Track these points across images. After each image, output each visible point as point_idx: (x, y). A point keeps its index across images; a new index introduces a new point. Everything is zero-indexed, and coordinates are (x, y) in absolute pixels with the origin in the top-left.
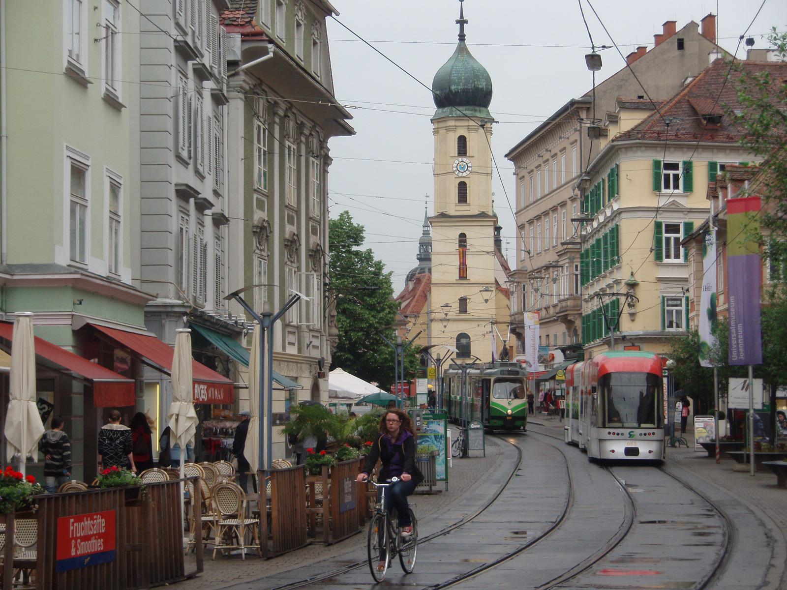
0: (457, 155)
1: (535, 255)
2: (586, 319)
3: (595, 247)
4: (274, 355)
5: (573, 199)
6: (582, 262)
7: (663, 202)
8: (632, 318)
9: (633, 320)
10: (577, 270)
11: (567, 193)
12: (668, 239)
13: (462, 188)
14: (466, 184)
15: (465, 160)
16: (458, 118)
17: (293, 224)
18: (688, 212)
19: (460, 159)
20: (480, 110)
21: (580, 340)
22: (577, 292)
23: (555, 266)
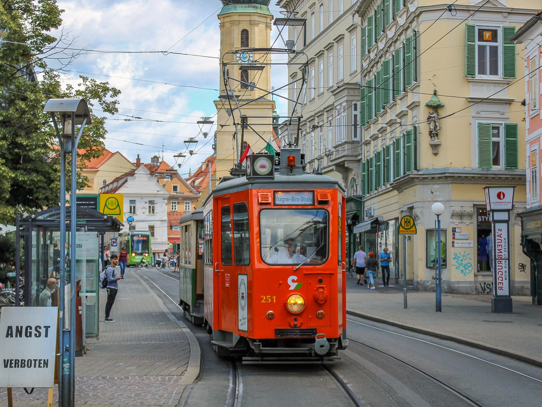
1: (308, 103)
5: (352, 29)
8: (436, 152)
9: (436, 154)
12: (482, 49)
18: (509, 13)
20: (261, 8)
22: (355, 136)
23: (330, 109)
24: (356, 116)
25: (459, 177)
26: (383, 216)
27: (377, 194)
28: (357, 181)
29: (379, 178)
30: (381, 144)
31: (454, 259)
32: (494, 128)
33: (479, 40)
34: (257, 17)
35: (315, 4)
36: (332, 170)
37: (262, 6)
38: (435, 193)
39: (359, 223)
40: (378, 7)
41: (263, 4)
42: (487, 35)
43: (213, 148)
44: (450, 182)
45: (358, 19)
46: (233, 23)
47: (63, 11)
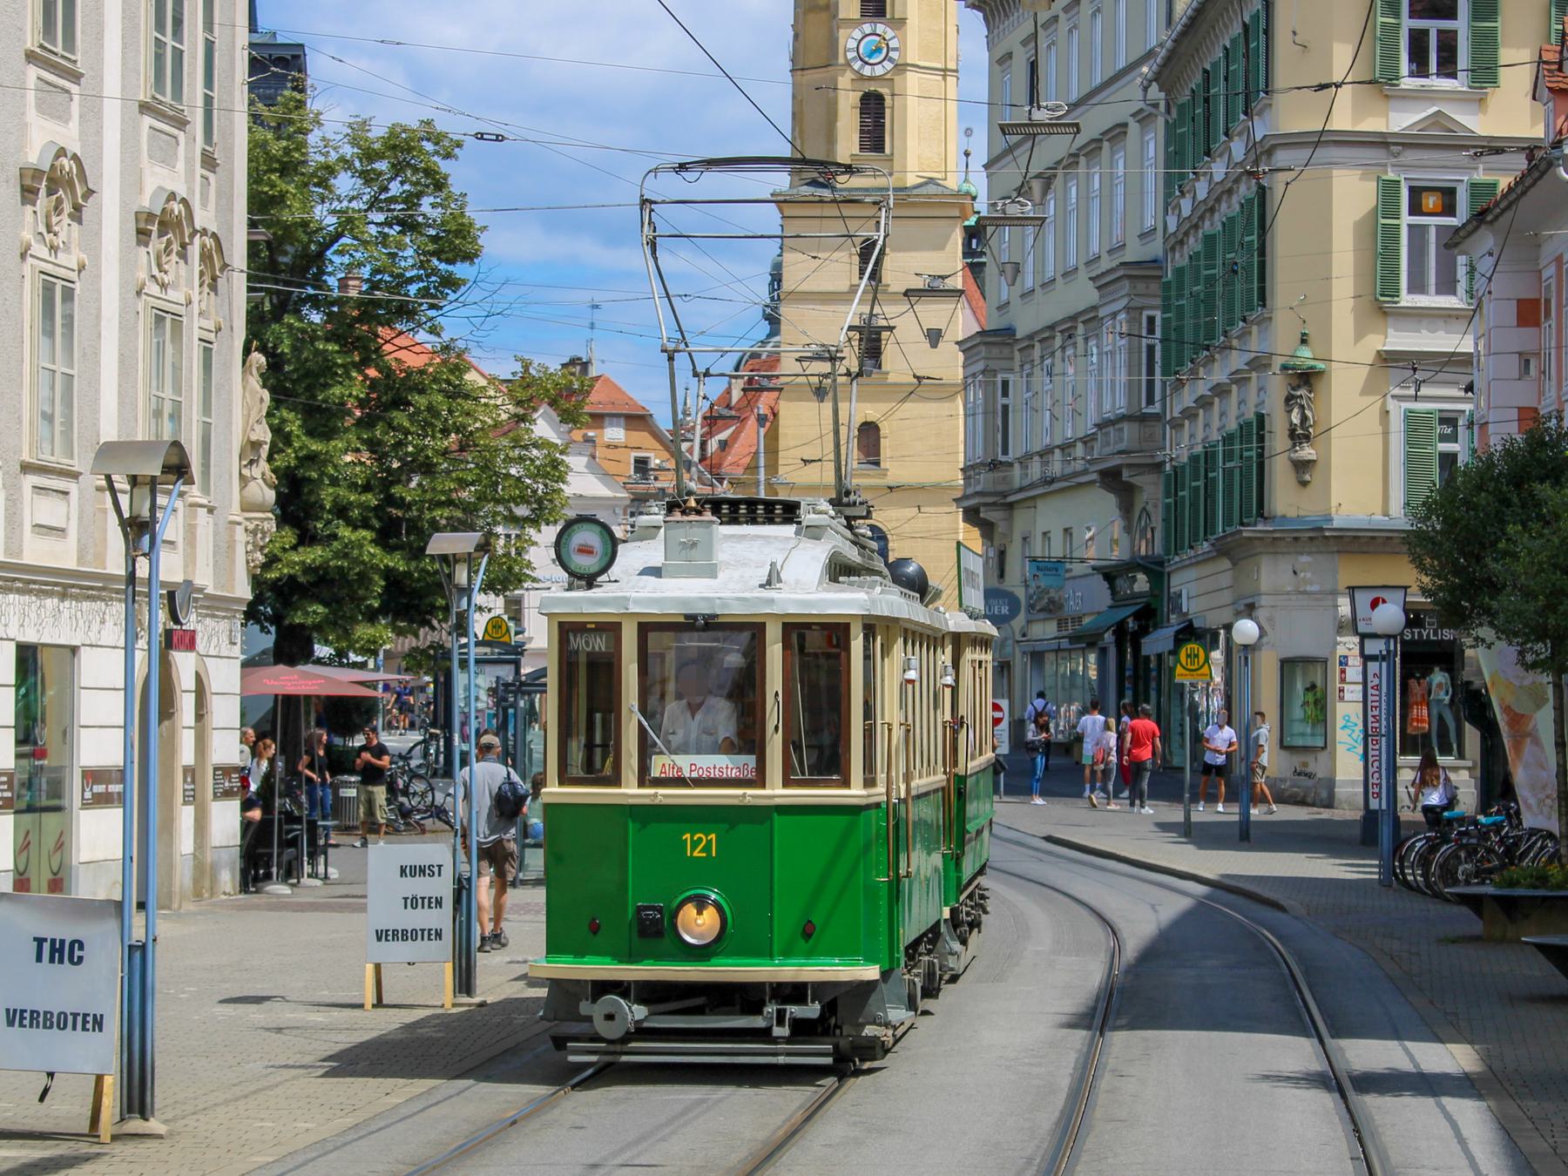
2: (1175, 480)
3: (1202, 255)
5: (1143, 118)
6: (1166, 308)
7: (1401, 120)
9: (1304, 484)
10: (1151, 331)
11: (1129, 98)
12: (1417, 232)
14: (883, 99)
15: (880, 28)
19: (867, 28)
21: (1158, 549)
22: (1150, 401)
23: (1090, 318)
25: (1355, 537)
27: (1193, 560)
29: (1231, 503)
31: (1343, 728)
32: (1443, 421)
33: (1411, 213)
35: (1057, 21)
38: (1302, 575)
39: (1156, 627)
42: (1431, 201)
44: (1335, 549)
45: (1155, 92)
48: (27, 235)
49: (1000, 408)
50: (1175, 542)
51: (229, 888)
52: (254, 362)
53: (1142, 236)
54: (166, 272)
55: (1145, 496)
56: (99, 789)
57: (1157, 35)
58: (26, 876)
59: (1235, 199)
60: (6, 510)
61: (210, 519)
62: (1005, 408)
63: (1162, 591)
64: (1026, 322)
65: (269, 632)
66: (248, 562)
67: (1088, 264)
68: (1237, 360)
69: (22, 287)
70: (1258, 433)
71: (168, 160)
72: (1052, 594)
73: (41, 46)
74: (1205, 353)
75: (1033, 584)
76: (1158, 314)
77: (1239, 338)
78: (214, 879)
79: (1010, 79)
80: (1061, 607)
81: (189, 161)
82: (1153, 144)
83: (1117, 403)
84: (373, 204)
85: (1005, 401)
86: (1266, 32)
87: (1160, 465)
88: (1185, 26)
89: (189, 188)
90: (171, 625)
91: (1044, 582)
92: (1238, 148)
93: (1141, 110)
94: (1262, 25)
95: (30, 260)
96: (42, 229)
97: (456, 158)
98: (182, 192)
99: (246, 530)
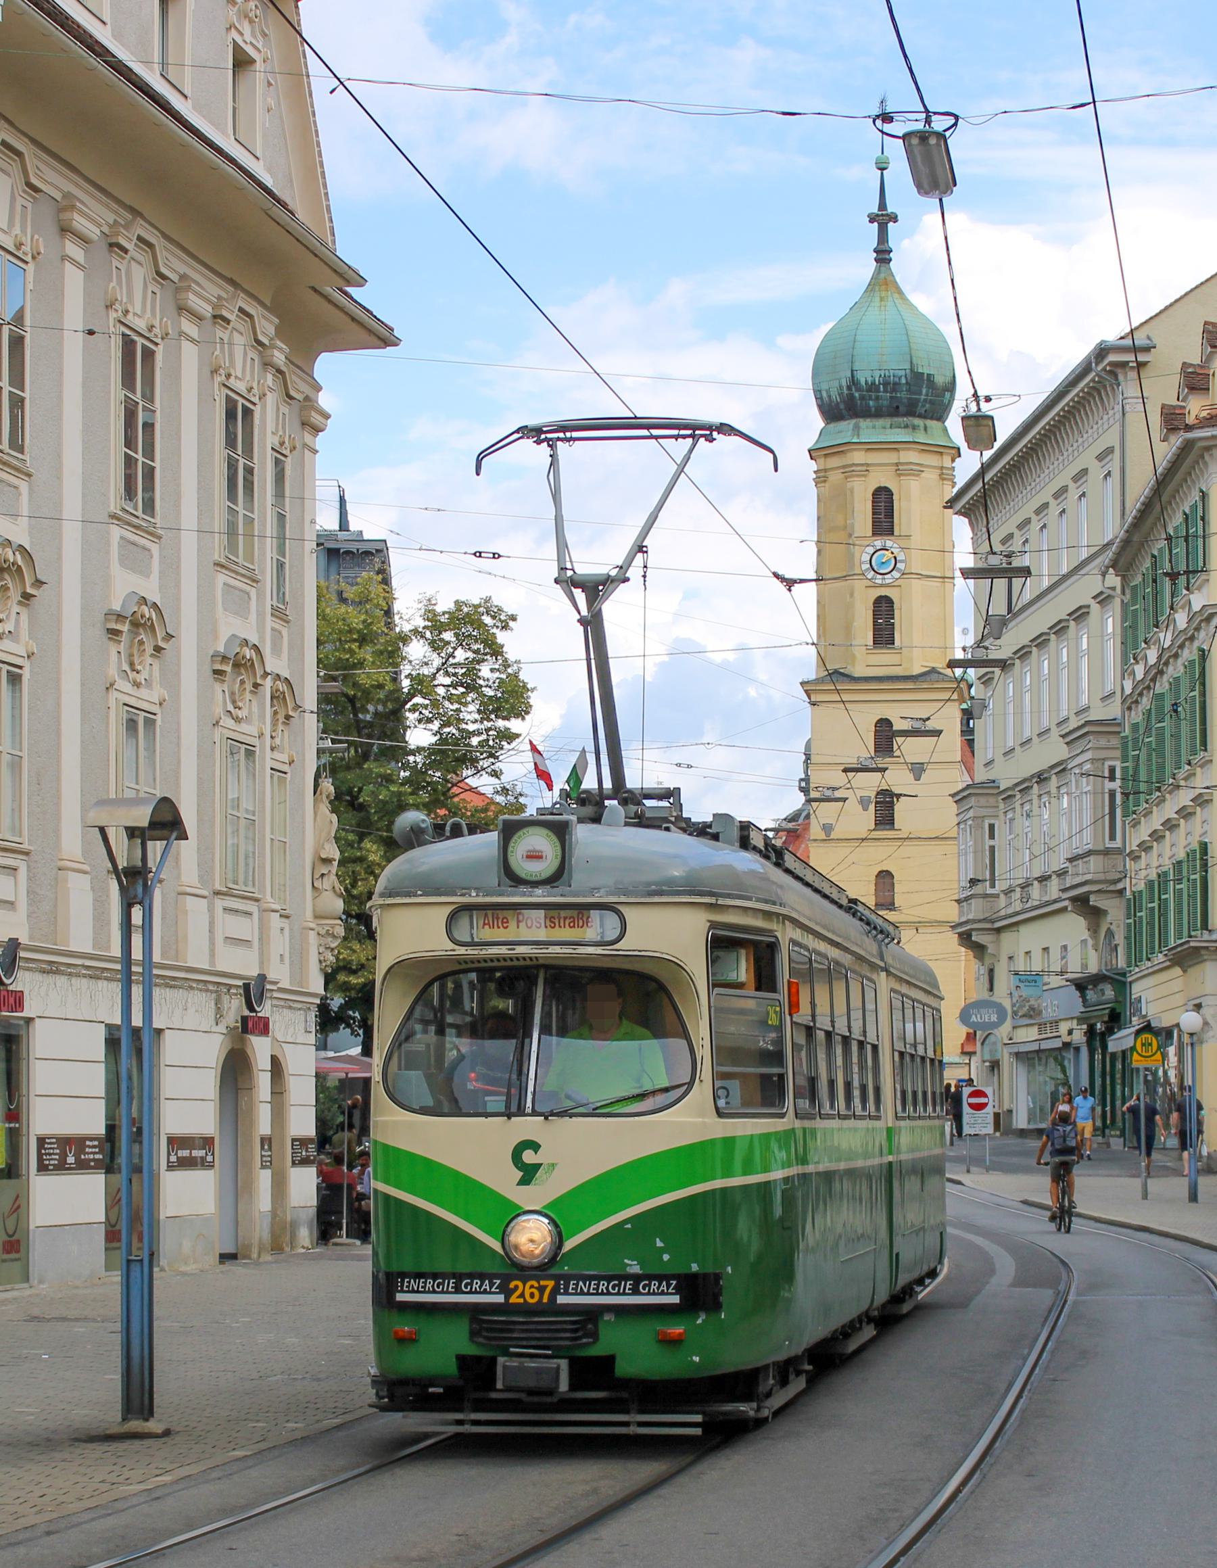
0: (870, 533)
2: (1134, 904)
4: (118, 967)
5: (1103, 599)
6: (1124, 759)
13: (884, 608)
15: (889, 544)
16: (872, 447)
17: (245, 617)
19: (879, 543)
20: (926, 429)
21: (1121, 963)
22: (1112, 837)
23: (1061, 769)
24: (1112, 794)
26: (1160, 1018)
28: (1116, 937)
29: (1181, 925)
30: (1185, 843)
34: (916, 453)
36: (1064, 909)
37: (929, 423)
39: (1120, 1029)
40: (1176, 529)
41: (932, 418)
43: (802, 789)
45: (1113, 580)
46: (849, 471)
47: (533, 690)
48: (113, 672)
49: (987, 848)
50: (1135, 957)
51: (307, 1243)
52: (324, 791)
53: (1104, 699)
54: (240, 709)
55: (1109, 918)
56: (184, 1153)
57: (1112, 528)
58: (117, 1228)
59: (1180, 661)
60: (95, 909)
61: (285, 923)
62: (992, 849)
63: (1125, 999)
64: (1007, 775)
65: (358, 1035)
66: (320, 962)
67: (1059, 724)
68: (1184, 798)
69: (107, 717)
70: (1201, 859)
71: (241, 611)
72: (1032, 1002)
73: (123, 510)
74: (1158, 794)
75: (1016, 994)
76: (1118, 765)
77: (1186, 779)
78: (293, 1236)
79: (1030, 670)
80: (1040, 1013)
81: (261, 615)
82: (1111, 623)
83: (1087, 841)
84: (442, 668)
85: (992, 843)
86: (1203, 519)
87: (1121, 892)
88: (1135, 518)
89: (260, 638)
90: (246, 1013)
91: (1026, 992)
92: (1181, 619)
93: (1102, 593)
94: (1200, 513)
95: (116, 694)
96: (126, 667)
97: (512, 630)
98: (254, 639)
99: (319, 934)
